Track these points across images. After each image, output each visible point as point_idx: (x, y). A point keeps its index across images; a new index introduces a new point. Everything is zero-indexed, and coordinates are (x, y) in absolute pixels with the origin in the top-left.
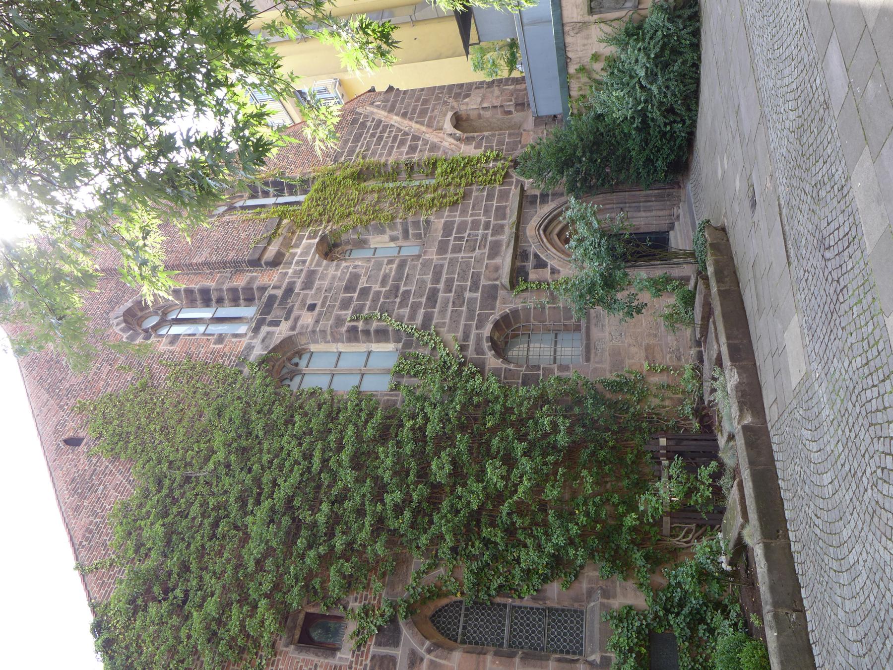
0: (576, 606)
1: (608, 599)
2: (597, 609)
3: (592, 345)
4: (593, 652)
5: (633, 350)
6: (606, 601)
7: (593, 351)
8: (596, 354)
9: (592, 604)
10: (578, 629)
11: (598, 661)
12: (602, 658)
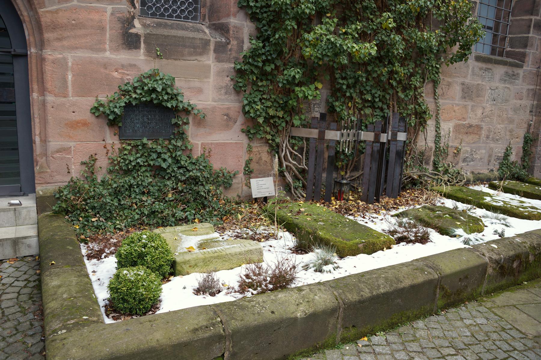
0: (205, 11)
1: (215, 51)
2: (201, 36)
3: (490, 66)
4: (144, 26)
5: (479, 112)
6: (212, 47)
7: (484, 65)
8: (481, 69)
9: (207, 31)
10: (158, 9)
11: (133, 31)
12: (137, 36)
